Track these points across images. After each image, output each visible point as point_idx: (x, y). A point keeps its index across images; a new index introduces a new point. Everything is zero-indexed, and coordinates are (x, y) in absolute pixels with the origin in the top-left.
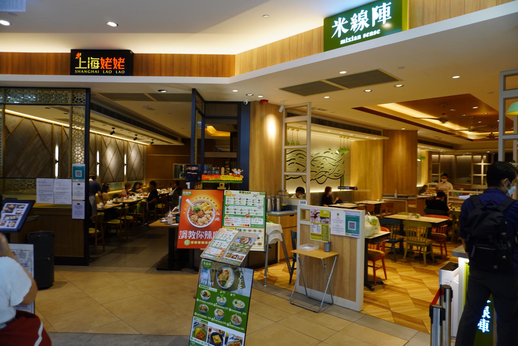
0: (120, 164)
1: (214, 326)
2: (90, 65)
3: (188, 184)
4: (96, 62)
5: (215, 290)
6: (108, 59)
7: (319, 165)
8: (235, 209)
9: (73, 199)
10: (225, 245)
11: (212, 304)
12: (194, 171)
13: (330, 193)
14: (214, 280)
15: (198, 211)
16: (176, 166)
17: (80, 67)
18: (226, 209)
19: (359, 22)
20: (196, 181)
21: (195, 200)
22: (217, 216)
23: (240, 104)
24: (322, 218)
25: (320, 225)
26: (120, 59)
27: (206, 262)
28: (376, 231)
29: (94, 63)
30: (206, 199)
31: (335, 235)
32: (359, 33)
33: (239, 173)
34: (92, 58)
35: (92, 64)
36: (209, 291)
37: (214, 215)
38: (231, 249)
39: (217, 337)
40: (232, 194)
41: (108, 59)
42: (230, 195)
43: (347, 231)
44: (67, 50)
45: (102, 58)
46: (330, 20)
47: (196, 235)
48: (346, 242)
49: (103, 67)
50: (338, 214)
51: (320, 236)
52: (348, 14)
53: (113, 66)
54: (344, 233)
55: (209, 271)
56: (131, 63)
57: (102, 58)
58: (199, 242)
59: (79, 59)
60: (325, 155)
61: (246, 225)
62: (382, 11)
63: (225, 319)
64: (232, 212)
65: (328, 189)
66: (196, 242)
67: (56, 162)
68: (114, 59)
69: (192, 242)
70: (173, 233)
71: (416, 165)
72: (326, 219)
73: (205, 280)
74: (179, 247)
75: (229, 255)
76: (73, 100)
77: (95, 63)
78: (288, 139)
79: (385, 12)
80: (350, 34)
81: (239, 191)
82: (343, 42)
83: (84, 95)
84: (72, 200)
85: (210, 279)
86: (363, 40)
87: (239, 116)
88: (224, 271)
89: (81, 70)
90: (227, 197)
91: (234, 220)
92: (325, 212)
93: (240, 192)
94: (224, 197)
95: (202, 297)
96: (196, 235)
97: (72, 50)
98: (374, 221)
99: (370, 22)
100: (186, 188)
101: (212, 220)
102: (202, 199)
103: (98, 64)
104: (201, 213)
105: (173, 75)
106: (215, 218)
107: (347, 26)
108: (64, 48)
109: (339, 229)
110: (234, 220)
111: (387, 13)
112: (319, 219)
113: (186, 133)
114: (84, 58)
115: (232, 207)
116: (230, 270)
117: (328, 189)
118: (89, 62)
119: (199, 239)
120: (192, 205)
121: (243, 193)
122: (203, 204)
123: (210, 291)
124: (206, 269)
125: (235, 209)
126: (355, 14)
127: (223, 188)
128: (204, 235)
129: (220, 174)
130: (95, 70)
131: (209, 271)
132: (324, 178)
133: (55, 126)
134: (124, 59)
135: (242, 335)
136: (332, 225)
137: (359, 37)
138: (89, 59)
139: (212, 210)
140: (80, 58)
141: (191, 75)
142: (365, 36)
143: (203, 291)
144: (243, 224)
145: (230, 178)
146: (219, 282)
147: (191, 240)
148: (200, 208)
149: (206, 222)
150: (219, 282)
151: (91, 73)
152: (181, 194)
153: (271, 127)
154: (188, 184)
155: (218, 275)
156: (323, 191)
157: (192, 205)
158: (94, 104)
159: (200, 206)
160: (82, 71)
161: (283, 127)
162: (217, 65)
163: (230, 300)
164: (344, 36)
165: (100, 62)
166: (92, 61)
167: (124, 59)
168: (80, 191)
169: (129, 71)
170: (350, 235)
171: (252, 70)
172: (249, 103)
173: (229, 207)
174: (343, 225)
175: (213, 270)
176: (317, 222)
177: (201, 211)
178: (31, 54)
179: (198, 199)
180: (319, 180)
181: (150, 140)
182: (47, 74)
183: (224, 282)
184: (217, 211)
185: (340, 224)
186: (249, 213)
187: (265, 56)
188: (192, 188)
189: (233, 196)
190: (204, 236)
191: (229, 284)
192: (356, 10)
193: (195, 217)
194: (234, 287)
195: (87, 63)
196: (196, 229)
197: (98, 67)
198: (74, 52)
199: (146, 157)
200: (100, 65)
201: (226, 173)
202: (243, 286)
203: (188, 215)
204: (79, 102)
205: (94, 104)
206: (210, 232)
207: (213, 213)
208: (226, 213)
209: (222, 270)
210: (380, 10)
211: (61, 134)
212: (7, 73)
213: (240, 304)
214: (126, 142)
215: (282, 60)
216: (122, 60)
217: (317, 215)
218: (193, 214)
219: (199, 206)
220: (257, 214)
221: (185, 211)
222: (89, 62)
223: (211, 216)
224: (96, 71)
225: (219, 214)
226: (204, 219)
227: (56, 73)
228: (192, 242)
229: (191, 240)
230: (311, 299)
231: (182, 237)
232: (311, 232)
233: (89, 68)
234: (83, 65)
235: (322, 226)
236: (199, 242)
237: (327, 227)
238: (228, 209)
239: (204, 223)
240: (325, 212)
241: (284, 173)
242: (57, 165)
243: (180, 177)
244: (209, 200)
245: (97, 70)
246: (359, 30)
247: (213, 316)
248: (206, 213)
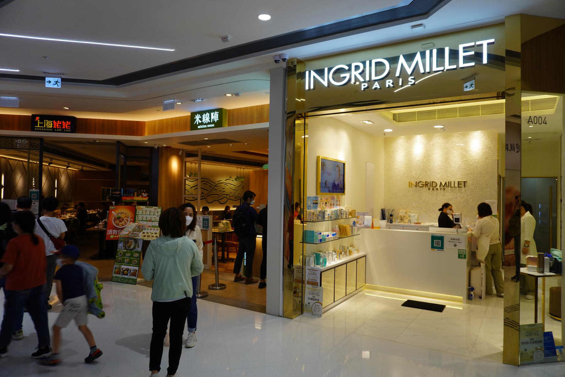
0: (52, 188)
1: (124, 267)
3: (114, 202)
5: (125, 251)
6: (58, 122)
7: (221, 189)
9: (539, 278)
10: (131, 230)
12: (118, 194)
13: (229, 211)
14: (125, 246)
15: (119, 218)
16: (103, 189)
20: (119, 202)
23: (151, 149)
26: (67, 122)
28: (228, 229)
32: (206, 124)
38: (134, 231)
39: (126, 271)
41: (58, 122)
46: (193, 114)
49: (55, 127)
52: (201, 113)
53: (62, 126)
56: (76, 125)
60: (227, 182)
63: (129, 263)
64: (140, 218)
65: (227, 208)
67: (2, 187)
68: (63, 122)
70: (103, 233)
74: (107, 239)
75: (132, 234)
77: (49, 124)
80: (202, 124)
82: (199, 127)
87: (155, 155)
94: (136, 210)
98: (227, 223)
99: (210, 120)
100: (112, 205)
102: (122, 211)
104: (121, 219)
105: (103, 134)
107: (201, 119)
113: (113, 161)
114: (42, 120)
115: (141, 216)
116: (133, 241)
117: (227, 208)
120: (116, 215)
124: (121, 242)
127: (135, 204)
129: (134, 196)
132: (225, 200)
133: (2, 159)
135: (137, 268)
137: (206, 126)
141: (116, 134)
142: (208, 126)
145: (140, 198)
147: (114, 235)
151: (47, 130)
152: (108, 209)
153: (174, 165)
154: (114, 202)
156: (223, 209)
157: (116, 215)
158: (46, 148)
161: (182, 163)
162: (135, 128)
163: (132, 254)
164: (200, 124)
165: (53, 123)
169: (73, 131)
170: (205, 229)
171: (155, 133)
172: (158, 148)
179: (120, 211)
180: (221, 201)
181: (80, 167)
183: (130, 247)
187: (163, 126)
188: (116, 204)
189: (142, 210)
191: (132, 247)
192: (205, 112)
193: (118, 222)
194: (134, 248)
197: (51, 127)
198: (34, 116)
199: (73, 180)
200: (53, 126)
201: (138, 196)
202: (138, 247)
205: (46, 148)
207: (129, 219)
211: (6, 165)
213: (137, 255)
214: (57, 169)
215: (172, 131)
216: (68, 123)
219: (120, 215)
226: (123, 223)
234: (40, 125)
241: (184, 196)
242: (2, 190)
243: (108, 200)
247: (124, 262)
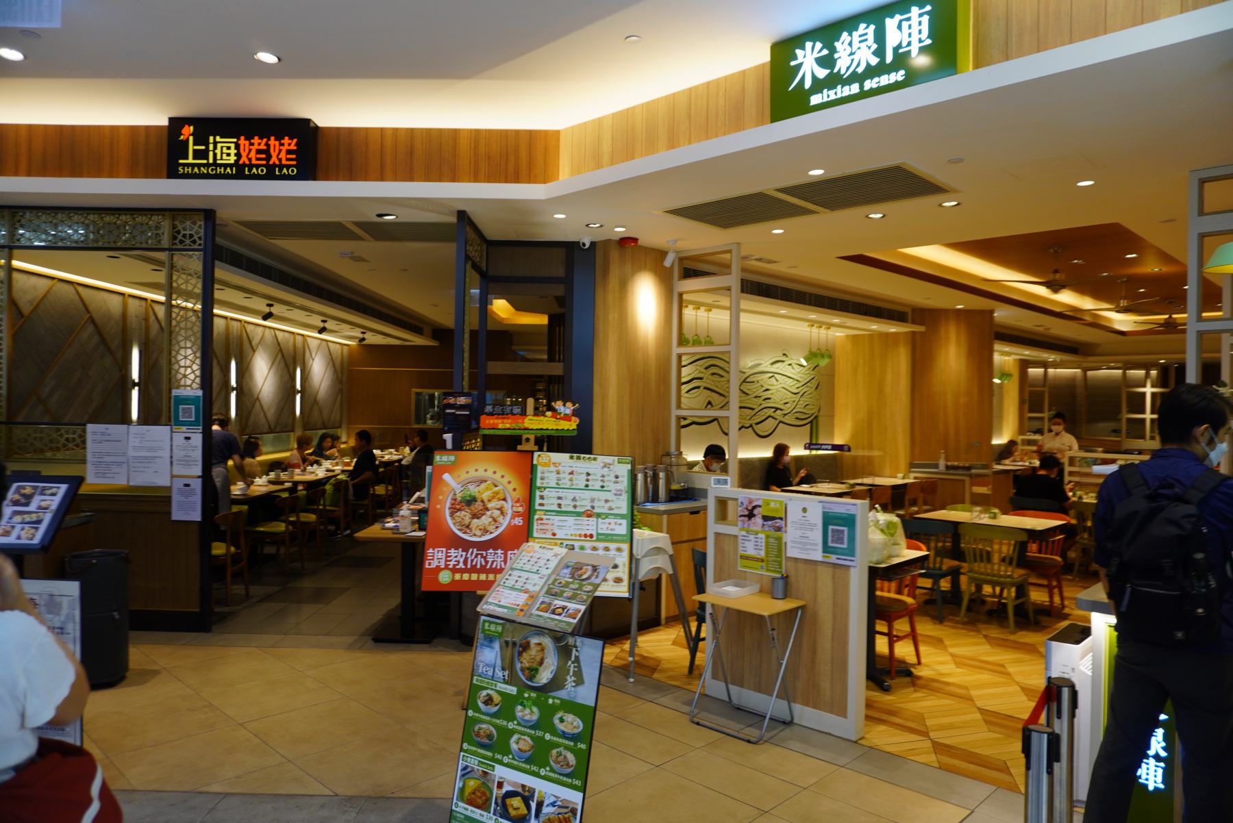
0: (287, 391)
1: (509, 776)
2: (215, 155)
3: (448, 437)
4: (229, 148)
5: (512, 690)
6: (256, 140)
7: (759, 393)
8: (560, 498)
9: (175, 473)
10: (536, 584)
11: (505, 723)
12: (462, 407)
13: (787, 459)
14: (509, 666)
15: (471, 501)
16: (418, 394)
17: (191, 160)
18: (537, 498)
19: (855, 51)
20: (466, 431)
21: (464, 476)
22: (516, 514)
23: (571, 248)
24: (766, 518)
25: (762, 536)
26: (286, 140)
27: (491, 623)
28: (895, 550)
29: (225, 150)
30: (490, 474)
31: (796, 560)
32: (856, 78)
33: (568, 412)
34: (218, 139)
35: (218, 151)
36: (497, 691)
37: (510, 513)
38: (550, 593)
39: (516, 802)
40: (553, 460)
41: (256, 140)
42: (546, 465)
43: (826, 549)
44: (159, 119)
45: (242, 138)
46: (785, 48)
47: (466, 559)
48: (825, 575)
49: (244, 159)
50: (805, 510)
51: (762, 561)
52: (828, 32)
53: (269, 157)
54: (818, 555)
55: (497, 645)
56: (312, 150)
57: (242, 138)
58: (474, 577)
59: (188, 140)
60: (774, 368)
61: (585, 536)
63: (536, 759)
64: (551, 504)
65: (781, 450)
66: (466, 577)
67: (134, 384)
68: (272, 141)
69: (458, 576)
70: (411, 553)
72: (775, 522)
73: (487, 665)
74: (426, 586)
75: (546, 608)
76: (175, 238)
77: (225, 150)
80: (834, 80)
81: (568, 455)
82: (815, 100)
83: (200, 227)
84: (172, 477)
85: (499, 662)
86: (863, 95)
87: (568, 275)
88: (532, 645)
89: (193, 165)
90: (540, 469)
91: (557, 524)
92: (772, 505)
93: (572, 458)
94: (533, 469)
95: (481, 705)
96: (466, 559)
97: (170, 119)
98: (890, 525)
99: (880, 52)
100: (442, 446)
101: (505, 523)
102: (481, 473)
103: (233, 151)
104: (478, 506)
105: (411, 178)
106: (513, 517)
107: (827, 62)
108: (152, 115)
109: (806, 544)
110: (557, 524)
112: (758, 520)
113: (444, 316)
114: (201, 139)
115: (553, 493)
116: (547, 641)
117: (781, 450)
118: (211, 147)
119: (474, 569)
120: (458, 488)
121: (579, 458)
122: (483, 486)
123: (499, 692)
124: (490, 639)
125: (560, 498)
126: (845, 34)
127: (530, 446)
128: (485, 558)
129: (524, 413)
130: (226, 166)
131: (497, 645)
132: (770, 424)
133: (131, 300)
134: (295, 141)
135: (575, 797)
136: (791, 535)
137: (855, 88)
138: (211, 139)
139: (504, 499)
140: (191, 138)
141: (454, 179)
142: (868, 85)
143: (484, 693)
144: (578, 532)
145: (547, 423)
146: (522, 670)
147: (454, 570)
148: (477, 495)
149: (491, 528)
150: (522, 670)
151: (218, 173)
152: (430, 461)
153: (645, 302)
154: (448, 437)
155: (520, 654)
156: (768, 453)
157: (458, 488)
158: (225, 248)
159: (476, 490)
160: (196, 170)
161: (673, 301)
162: (518, 155)
163: (547, 713)
164: (818, 86)
165: (237, 146)
166: (219, 146)
167: (295, 141)
168: (190, 453)
169: (308, 168)
170: (833, 558)
171: (599, 166)
172: (593, 244)
173: (545, 493)
174: (817, 536)
175: (507, 643)
176: (755, 528)
177: (479, 503)
178: (73, 128)
179: (472, 474)
180: (758, 428)
181: (357, 333)
182: (111, 175)
183: (532, 672)
184: (518, 501)
185: (808, 533)
186: (593, 507)
187: (630, 133)
188: (458, 446)
189: (554, 467)
190: (487, 562)
191: (544, 676)
192: (849, 23)
193: (465, 515)
194: (556, 683)
195: (207, 150)
196: (465, 545)
197: (232, 159)
198: (176, 124)
199: (347, 372)
200: (238, 155)
201: (538, 412)
202: (579, 681)
203: (447, 512)
204: (188, 241)
205: (225, 248)
206: (499, 551)
207: (508, 506)
208: (537, 507)
209: (528, 643)
211: (146, 319)
212: (16, 174)
213: (572, 724)
214: (299, 339)
215: (672, 144)
216: (290, 143)
217: (755, 512)
218: (459, 510)
219: (473, 490)
220: (611, 509)
221: (439, 502)
222: (211, 147)
223: (502, 513)
224: (228, 170)
225: (520, 509)
226: (485, 520)
227: (133, 173)
228: (458, 576)
229: (454, 570)
230: (740, 711)
231: (434, 564)
232: (741, 552)
233: (211, 161)
234: (197, 154)
235: (767, 537)
236: (474, 577)
237: (779, 539)
238: (542, 497)
239: (486, 531)
240: (772, 505)
241: (675, 412)
242: (135, 393)
243: (429, 422)
244: (498, 476)
245: (231, 166)
246: (854, 72)
247: (507, 751)
248: (489, 505)
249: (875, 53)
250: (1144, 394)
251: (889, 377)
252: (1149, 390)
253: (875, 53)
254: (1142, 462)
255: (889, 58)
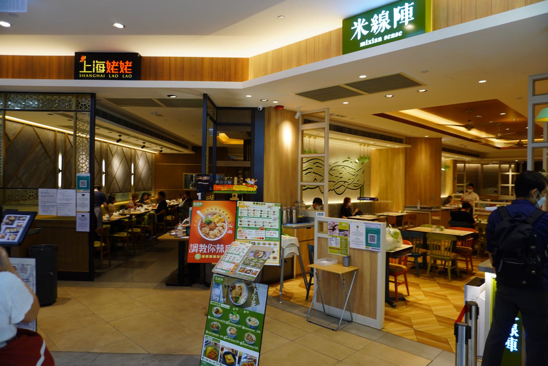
0: (127, 174)
1: (226, 345)
2: (96, 69)
3: (199, 194)
4: (102, 66)
5: (228, 307)
6: (114, 62)
7: (337, 175)
8: (249, 221)
9: (78, 210)
10: (238, 260)
11: (224, 322)
12: (205, 181)
13: (350, 204)
14: (226, 296)
15: (209, 223)
16: (186, 175)
17: (85, 71)
18: (239, 221)
19: (380, 23)
20: (207, 192)
21: (206, 212)
22: (229, 229)
23: (254, 110)
24: (340, 230)
25: (339, 238)
26: (127, 62)
27: (218, 277)
28: (398, 244)
29: (100, 67)
30: (218, 211)
31: (354, 249)
32: (380, 35)
33: (252, 183)
34: (97, 62)
35: (97, 67)
36: (221, 307)
37: (227, 228)
38: (244, 264)
39: (229, 357)
40: (246, 205)
41: (114, 62)
42: (243, 207)
43: (367, 244)
44: (71, 53)
45: (108, 61)
46: (349, 21)
47: (207, 249)
48: (367, 256)
49: (108, 71)
50: (358, 227)
51: (339, 249)
52: (368, 14)
53: (120, 70)
54: (363, 247)
55: (221, 287)
56: (139, 67)
57: (108, 61)
58: (211, 256)
59: (83, 62)
60: (344, 164)
61: (260, 238)
62: (404, 12)
63: (238, 338)
64: (245, 224)
65: (347, 200)
66: (207, 256)
67: (60, 171)
68: (121, 63)
69: (203, 256)
70: (183, 246)
71: (441, 175)
72: (345, 232)
73: (217, 296)
74: (189, 261)
75: (243, 270)
76: (78, 106)
77: (100, 67)
78: (304, 147)
79: (407, 12)
80: (371, 36)
81: (252, 202)
82: (362, 44)
83: (89, 101)
84: (77, 212)
85: (222, 295)
86: (384, 42)
87: (252, 122)
88: (236, 287)
89: (86, 74)
90: (240, 208)
91: (247, 233)
92: (343, 225)
93: (254, 203)
94: (237, 208)
95: (214, 314)
96: (207, 249)
97: (76, 53)
98: (395, 233)
99: (391, 23)
100: (196, 198)
101: (224, 232)
102: (214, 210)
103: (103, 67)
104: (212, 225)
105: (183, 79)
106: (228, 230)
107: (368, 27)
108: (67, 51)
109: (358, 242)
110: (247, 233)
111: (409, 14)
112: (337, 231)
113: (197, 140)
114: (89, 62)
115: (246, 219)
116: (243, 285)
117: (347, 200)
118: (94, 65)
119: (211, 253)
120: (204, 217)
121: (257, 204)
122: (215, 216)
123: (222, 308)
124: (218, 284)
125: (249, 221)
126: (376, 15)
127: (236, 198)
128: (216, 248)
129: (233, 184)
130: (100, 74)
131: (221, 287)
132: (342, 188)
133: (58, 134)
134: (131, 63)
135: (256, 355)
136: (352, 238)
137: (380, 39)
138: (94, 62)
139: (224, 222)
140: (85, 61)
141: (202, 79)
142: (386, 38)
143: (215, 308)
144: (257, 237)
145: (243, 188)
146: (232, 298)
147: (202, 254)
148: (212, 220)
149: (218, 235)
150: (232, 298)
151: (97, 77)
152: (191, 205)
153: (287, 134)
154: (199, 194)
155: (231, 291)
156: (342, 202)
157: (204, 217)
158: (100, 110)
159: (212, 218)
160: (87, 75)
161: (299, 134)
162: (230, 69)
163: (243, 317)
164: (364, 38)
165: (105, 65)
166: (97, 65)
167: (131, 63)
168: (85, 202)
169: (137, 75)
170: (370, 248)
171: (266, 74)
172: (264, 108)
173: (242, 219)
174: (363, 238)
175: (225, 286)
176: (335, 235)
177: (213, 224)
178: (32, 57)
179: (210, 211)
180: (337, 190)
181: (159, 148)
182: (49, 78)
183: (237, 299)
184: (230, 223)
185: (359, 237)
186: (263, 226)
187: (280, 59)
188: (203, 198)
189: (246, 208)
190: (216, 250)
191: (242, 301)
192: (377, 10)
193: (207, 229)
194: (247, 304)
195: (92, 67)
196: (207, 243)
197: (103, 71)
198: (78, 55)
199: (154, 166)
200: (106, 69)
201: (239, 183)
202: (258, 303)
203: (199, 228)
204: (83, 107)
205: (100, 110)
206: (222, 245)
207: (226, 225)
208: (239, 226)
209: (235, 286)
210: (402, 11)
211: (65, 142)
212: (7, 77)
213: (254, 322)
214: (133, 151)
215: (299, 64)
216: (129, 64)
217: (336, 228)
218: (204, 227)
219: (210, 218)
220: (271, 226)
221: (195, 223)
222: (94, 65)
223: (223, 228)
224: (102, 76)
225: (231, 226)
226: (216, 231)
227: (59, 77)
228: (203, 256)
229: (202, 254)
230: (329, 316)
231: (193, 251)
232: (329, 246)
233: (94, 72)
234: (88, 69)
235: (341, 239)
236: (211, 256)
237: (346, 240)
238: (241, 221)
239: (216, 236)
240: (343, 225)
241: (300, 183)
242: (60, 175)
243: (191, 188)
244: (221, 212)
245: (103, 74)
246: (380, 32)
247: (225, 334)
248: (218, 225)
249: (389, 24)
250: (508, 175)
251: (395, 168)
252: (510, 173)
253: (389, 24)
254: (508, 206)
255: (395, 26)
